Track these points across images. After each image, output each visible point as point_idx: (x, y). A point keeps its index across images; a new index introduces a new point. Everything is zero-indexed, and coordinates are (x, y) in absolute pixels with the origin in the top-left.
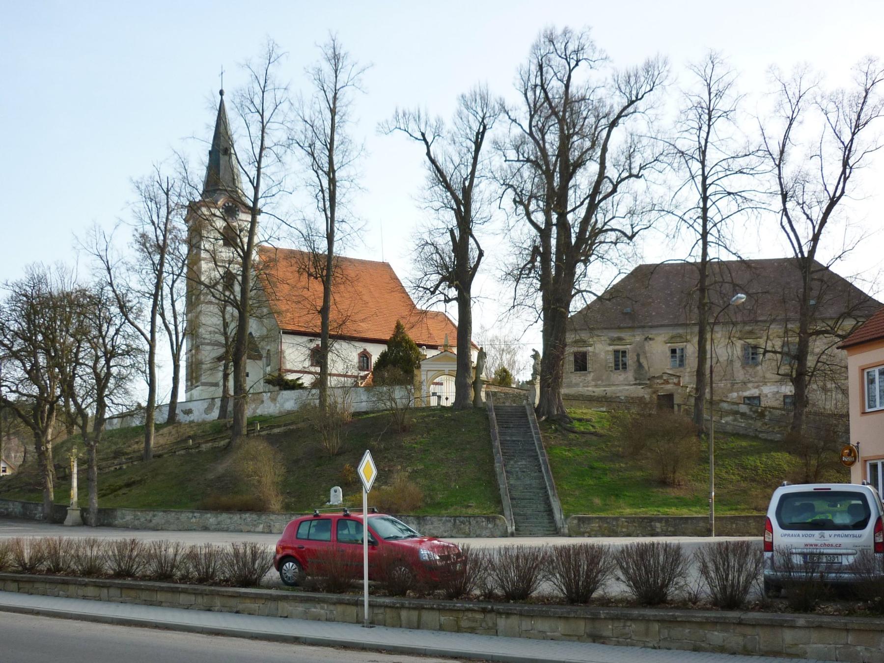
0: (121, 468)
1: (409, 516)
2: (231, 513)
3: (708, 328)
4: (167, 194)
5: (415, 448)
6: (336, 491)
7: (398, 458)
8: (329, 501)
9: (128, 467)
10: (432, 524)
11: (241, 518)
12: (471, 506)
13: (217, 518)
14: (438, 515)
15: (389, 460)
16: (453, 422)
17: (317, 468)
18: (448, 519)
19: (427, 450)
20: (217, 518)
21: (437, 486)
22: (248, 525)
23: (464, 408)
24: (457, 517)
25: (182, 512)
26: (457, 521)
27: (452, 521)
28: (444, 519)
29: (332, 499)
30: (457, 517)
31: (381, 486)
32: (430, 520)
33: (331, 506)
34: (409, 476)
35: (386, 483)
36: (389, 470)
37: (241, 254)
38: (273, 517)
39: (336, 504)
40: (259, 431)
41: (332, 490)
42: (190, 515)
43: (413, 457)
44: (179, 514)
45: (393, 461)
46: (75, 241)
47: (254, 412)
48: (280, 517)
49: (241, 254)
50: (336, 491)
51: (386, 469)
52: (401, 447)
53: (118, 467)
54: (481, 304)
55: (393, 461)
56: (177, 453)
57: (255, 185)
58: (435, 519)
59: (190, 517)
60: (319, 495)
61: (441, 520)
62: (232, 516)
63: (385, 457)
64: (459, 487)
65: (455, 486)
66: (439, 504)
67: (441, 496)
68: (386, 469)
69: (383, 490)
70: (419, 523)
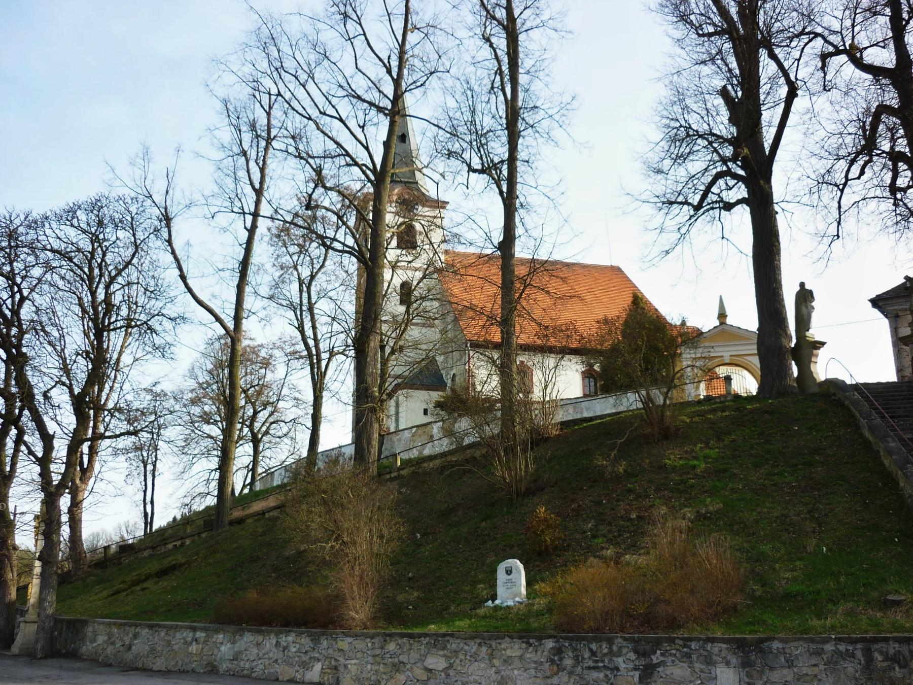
0: (182, 545)
1: (713, 640)
2: (259, 632)
3: (525, 640)
4: (269, 114)
5: (694, 467)
6: (509, 572)
7: (658, 490)
8: (494, 597)
9: (193, 542)
10: (790, 664)
11: (278, 644)
12: (898, 603)
13: (234, 643)
14: (804, 634)
15: (638, 497)
16: (767, 416)
17: (483, 524)
18: (842, 647)
19: (725, 471)
20: (234, 643)
21: (766, 548)
22: (290, 665)
23: (784, 392)
24: (875, 640)
25: (176, 628)
26: (878, 657)
27: (859, 654)
28: (829, 647)
29: (501, 590)
30: (875, 640)
31: (623, 555)
32: (783, 652)
33: (497, 608)
34: (690, 530)
35: (634, 548)
36: (638, 517)
37: (372, 178)
38: (344, 643)
39: (510, 603)
40: (399, 469)
41: (501, 568)
42: (189, 635)
43: (692, 486)
44: (172, 632)
45: (647, 496)
46: (111, 175)
47: (421, 453)
48: (360, 644)
49: (372, 178)
50: (509, 572)
51: (634, 516)
52: (662, 468)
53: (178, 543)
54: (788, 215)
55: (647, 496)
56: (267, 516)
57: (395, 75)
58: (798, 649)
59: (189, 639)
60: (474, 583)
61: (819, 653)
62: (260, 638)
63: (630, 491)
64: (829, 549)
65: (817, 546)
66: (788, 596)
67: (788, 575)
68: (634, 516)
69: (628, 564)
70: (746, 664)
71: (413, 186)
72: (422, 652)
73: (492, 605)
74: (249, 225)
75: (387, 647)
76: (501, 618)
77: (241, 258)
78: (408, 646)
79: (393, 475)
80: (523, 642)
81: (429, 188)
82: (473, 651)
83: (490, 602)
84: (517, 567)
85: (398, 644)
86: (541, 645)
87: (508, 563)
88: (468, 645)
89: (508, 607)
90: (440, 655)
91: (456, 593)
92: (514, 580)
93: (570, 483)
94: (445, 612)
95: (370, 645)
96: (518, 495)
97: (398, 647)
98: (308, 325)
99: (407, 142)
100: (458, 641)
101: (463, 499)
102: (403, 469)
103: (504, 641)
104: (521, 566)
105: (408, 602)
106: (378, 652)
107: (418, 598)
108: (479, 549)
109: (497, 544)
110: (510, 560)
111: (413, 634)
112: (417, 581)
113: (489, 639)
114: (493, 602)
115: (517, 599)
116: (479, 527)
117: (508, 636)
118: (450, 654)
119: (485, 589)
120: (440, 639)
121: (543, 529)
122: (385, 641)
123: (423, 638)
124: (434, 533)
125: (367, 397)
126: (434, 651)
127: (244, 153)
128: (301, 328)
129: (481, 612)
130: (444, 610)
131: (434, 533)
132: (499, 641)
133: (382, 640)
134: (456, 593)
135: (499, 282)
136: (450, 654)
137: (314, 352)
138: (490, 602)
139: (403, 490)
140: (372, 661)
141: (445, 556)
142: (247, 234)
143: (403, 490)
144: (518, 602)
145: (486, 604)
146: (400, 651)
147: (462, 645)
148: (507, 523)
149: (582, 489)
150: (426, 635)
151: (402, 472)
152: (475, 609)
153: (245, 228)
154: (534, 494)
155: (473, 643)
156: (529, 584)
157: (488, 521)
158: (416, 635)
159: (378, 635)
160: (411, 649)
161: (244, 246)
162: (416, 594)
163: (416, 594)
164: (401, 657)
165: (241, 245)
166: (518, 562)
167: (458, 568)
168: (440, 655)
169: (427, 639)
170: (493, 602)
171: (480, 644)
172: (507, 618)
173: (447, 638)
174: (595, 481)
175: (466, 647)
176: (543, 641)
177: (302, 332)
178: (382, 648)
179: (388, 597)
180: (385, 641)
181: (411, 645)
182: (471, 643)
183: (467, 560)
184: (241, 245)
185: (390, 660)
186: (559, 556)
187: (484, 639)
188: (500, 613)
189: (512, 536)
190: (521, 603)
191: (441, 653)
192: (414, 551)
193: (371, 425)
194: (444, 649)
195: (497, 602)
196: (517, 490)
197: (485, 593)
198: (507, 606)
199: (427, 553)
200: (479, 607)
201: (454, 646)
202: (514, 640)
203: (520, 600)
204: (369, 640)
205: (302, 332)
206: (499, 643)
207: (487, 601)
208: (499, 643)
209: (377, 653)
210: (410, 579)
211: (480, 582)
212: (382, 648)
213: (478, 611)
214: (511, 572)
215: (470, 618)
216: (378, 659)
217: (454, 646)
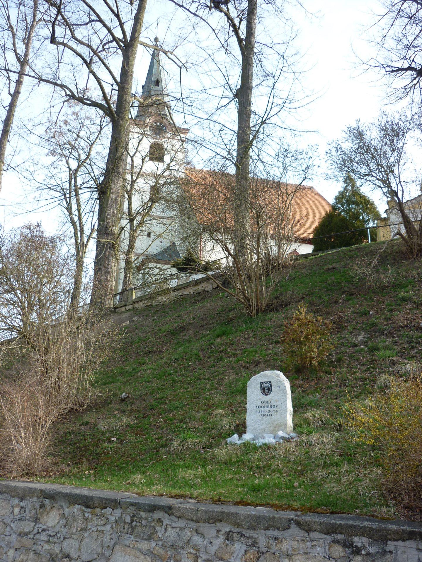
3: (340, 537)
6: (266, 389)
8: (241, 429)
17: (219, 340)
33: (248, 448)
39: (270, 440)
50: (266, 389)
60: (209, 407)
63: (404, 299)
71: (165, 116)
72: (107, 540)
73: (239, 442)
74: (12, 91)
75: (44, 518)
76: (258, 467)
77: (4, 118)
78: (79, 524)
79: (127, 308)
80: (336, 542)
81: (178, 119)
82: (213, 549)
83: (236, 436)
84: (280, 384)
85: (63, 516)
86: (384, 553)
87: (264, 376)
88: (203, 536)
89: (267, 446)
90: (140, 551)
91: (181, 421)
92: (273, 403)
93: (320, 297)
94: (163, 450)
95: (16, 510)
96: (258, 310)
97: (63, 522)
98: (74, 207)
99: (160, 86)
100: (181, 523)
101: (194, 319)
102: (137, 302)
103: (287, 533)
104: (287, 384)
105: (113, 431)
106: (28, 526)
107: (128, 426)
108: (213, 366)
109: (238, 361)
110: (268, 372)
111: (92, 498)
112: (132, 403)
113: (252, 527)
114: (240, 436)
115: (281, 433)
116: (213, 344)
117: (297, 523)
118: (161, 552)
119: (226, 416)
120: (143, 515)
121: (307, 335)
122: (42, 506)
123: (109, 510)
124: (160, 351)
125: (106, 234)
126: (128, 540)
127: (11, 28)
128: (69, 209)
129: (221, 452)
130: (162, 446)
131: (160, 351)
132: (275, 533)
133: (37, 505)
134: (181, 421)
135: (236, 128)
136: (161, 552)
137: (78, 228)
138: (236, 436)
139: (135, 319)
140: (17, 545)
141: (170, 374)
142: (10, 98)
143: (135, 319)
144: (283, 438)
145: (229, 440)
146: (65, 531)
147: (188, 533)
148: (248, 338)
149: (336, 302)
150: (115, 504)
151: (137, 306)
152: (211, 446)
153: (9, 93)
154: (277, 310)
155: (213, 532)
156: (297, 407)
157: (224, 337)
158: (97, 502)
159: (32, 492)
160: (86, 529)
161: (7, 108)
162: (125, 420)
163: (125, 420)
164: (65, 543)
165: (4, 107)
166: (281, 374)
167: (186, 389)
168: (140, 551)
169: (118, 512)
170: (240, 436)
171: (229, 537)
172: (269, 466)
173: (158, 515)
174: (351, 295)
175: (197, 540)
176: (391, 546)
177: (70, 213)
178: (36, 520)
179: (87, 423)
180: (42, 506)
181: (86, 520)
182: (210, 531)
183: (199, 379)
184: (4, 107)
185: (46, 547)
186: (330, 373)
187: (239, 525)
188: (254, 457)
189: (256, 352)
190: (288, 440)
191: (144, 546)
192: (134, 369)
193: (110, 261)
194: (150, 538)
195: (247, 437)
196: (257, 305)
197: (225, 421)
198: (265, 444)
199: (149, 372)
200: (218, 445)
201: (171, 534)
202: (313, 535)
203: (286, 436)
204: (16, 501)
205: (70, 213)
206: (276, 539)
207: (230, 435)
208: (276, 539)
209: (26, 530)
210: (123, 400)
211: (216, 406)
212: (36, 520)
213: (217, 451)
214: (269, 389)
215: (204, 463)
216: (27, 541)
217: (171, 534)
